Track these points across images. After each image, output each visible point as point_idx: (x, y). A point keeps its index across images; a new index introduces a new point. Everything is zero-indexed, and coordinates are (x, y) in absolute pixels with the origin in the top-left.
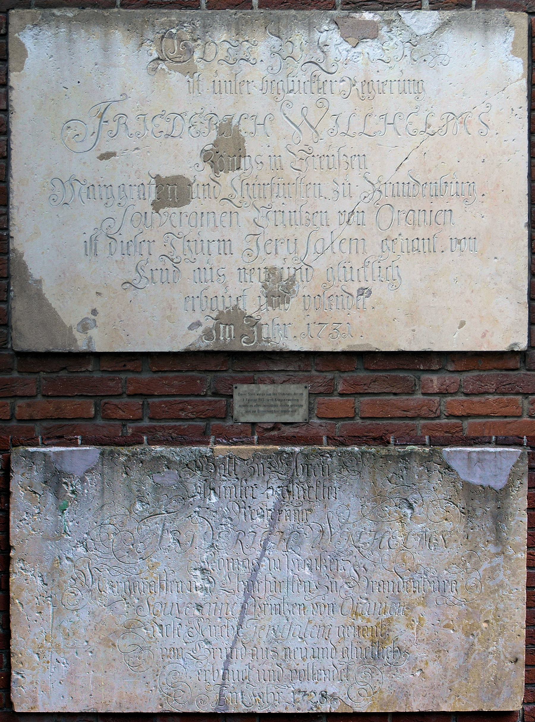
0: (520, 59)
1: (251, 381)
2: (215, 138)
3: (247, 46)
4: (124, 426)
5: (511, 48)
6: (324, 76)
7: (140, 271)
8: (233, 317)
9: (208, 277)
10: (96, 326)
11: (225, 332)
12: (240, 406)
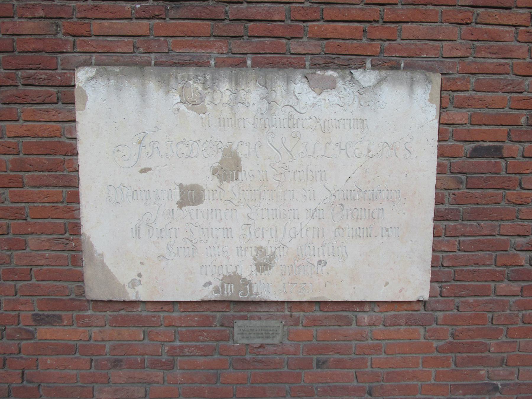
0: (434, 105)
1: (244, 318)
2: (220, 158)
3: (243, 94)
4: (162, 345)
5: (429, 98)
6: (297, 116)
7: (170, 248)
8: (233, 279)
9: (216, 253)
10: (237, 179)
11: (227, 288)
12: (238, 334)
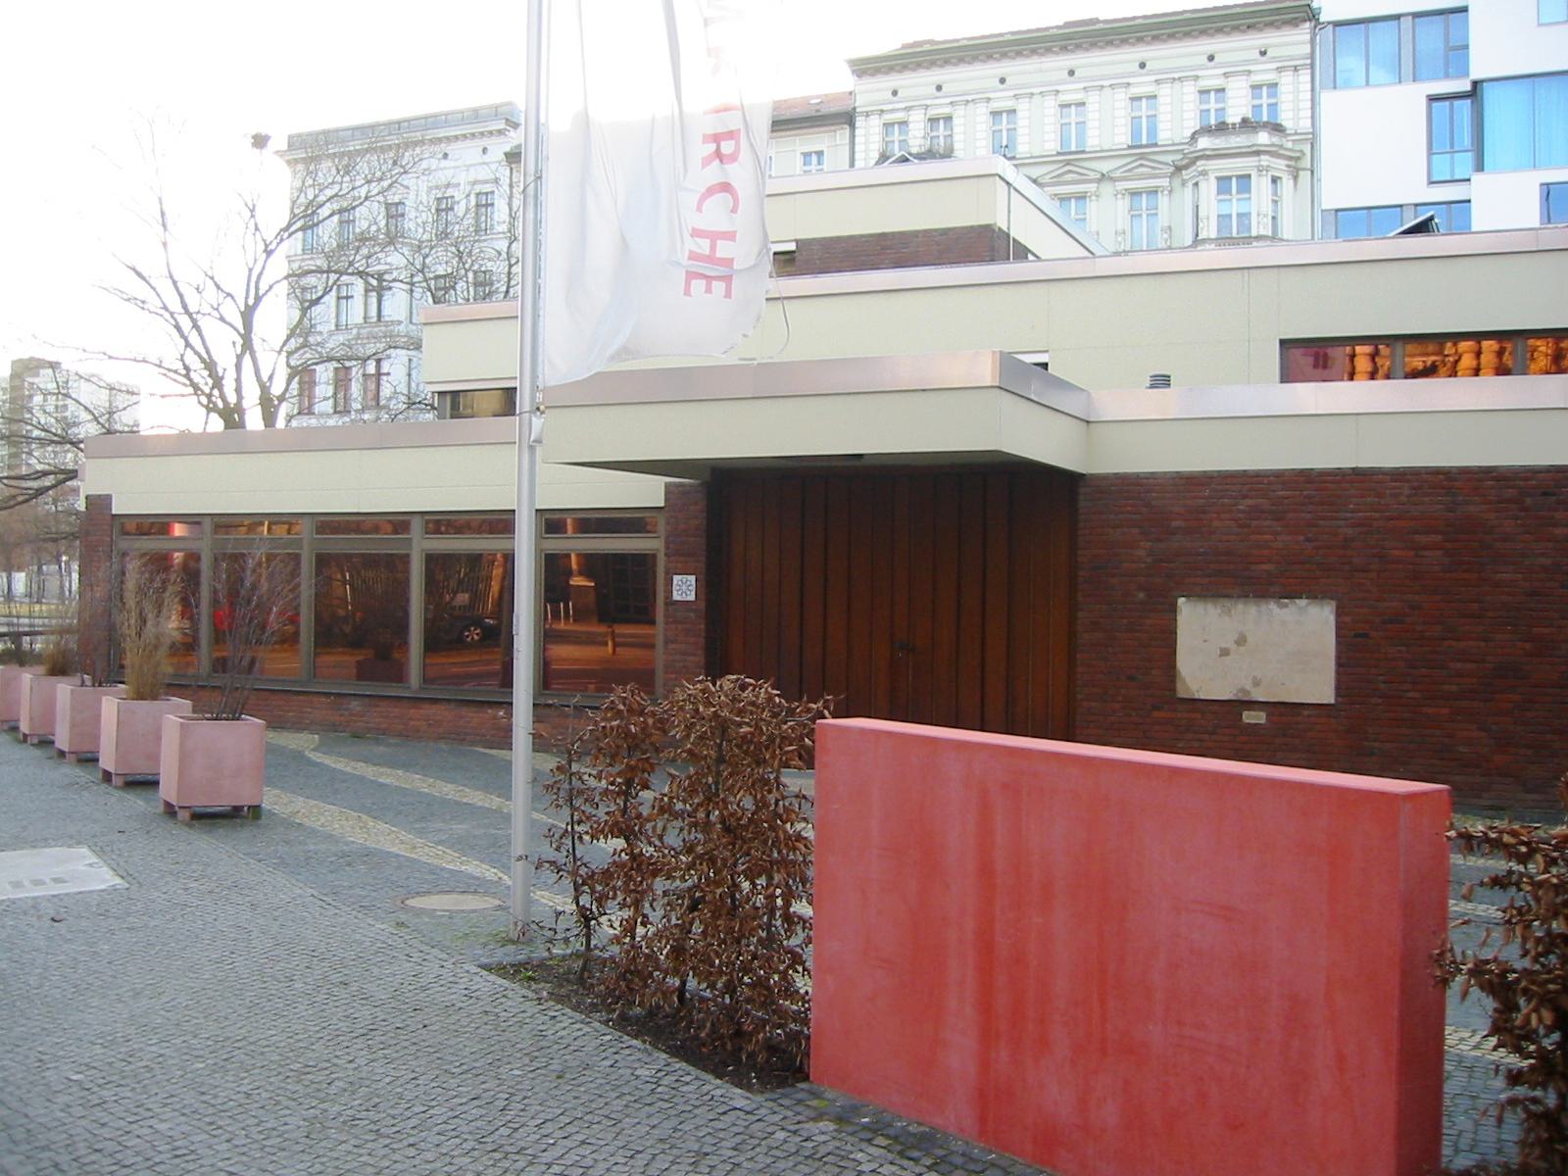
8: (1243, 690)
